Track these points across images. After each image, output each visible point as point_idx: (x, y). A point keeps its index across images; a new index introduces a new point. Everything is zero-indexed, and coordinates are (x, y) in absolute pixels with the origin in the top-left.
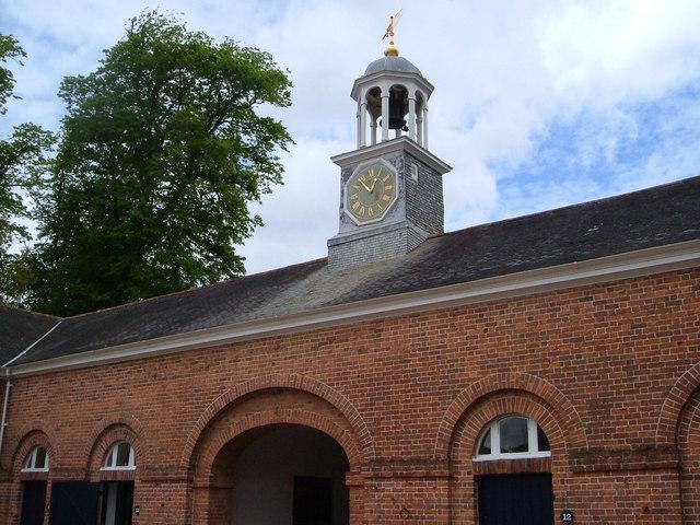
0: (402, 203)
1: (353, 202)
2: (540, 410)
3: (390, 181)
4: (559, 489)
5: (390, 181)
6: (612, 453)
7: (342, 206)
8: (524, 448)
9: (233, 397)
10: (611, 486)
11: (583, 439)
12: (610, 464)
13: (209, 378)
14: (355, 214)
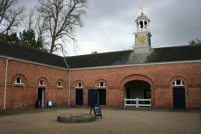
0: (148, 43)
1: (138, 42)
2: (183, 79)
3: (145, 39)
4: (186, 90)
5: (145, 39)
6: (194, 85)
7: (136, 42)
8: (180, 84)
9: (128, 75)
10: (193, 89)
11: (190, 83)
12: (194, 86)
13: (123, 72)
14: (138, 44)
